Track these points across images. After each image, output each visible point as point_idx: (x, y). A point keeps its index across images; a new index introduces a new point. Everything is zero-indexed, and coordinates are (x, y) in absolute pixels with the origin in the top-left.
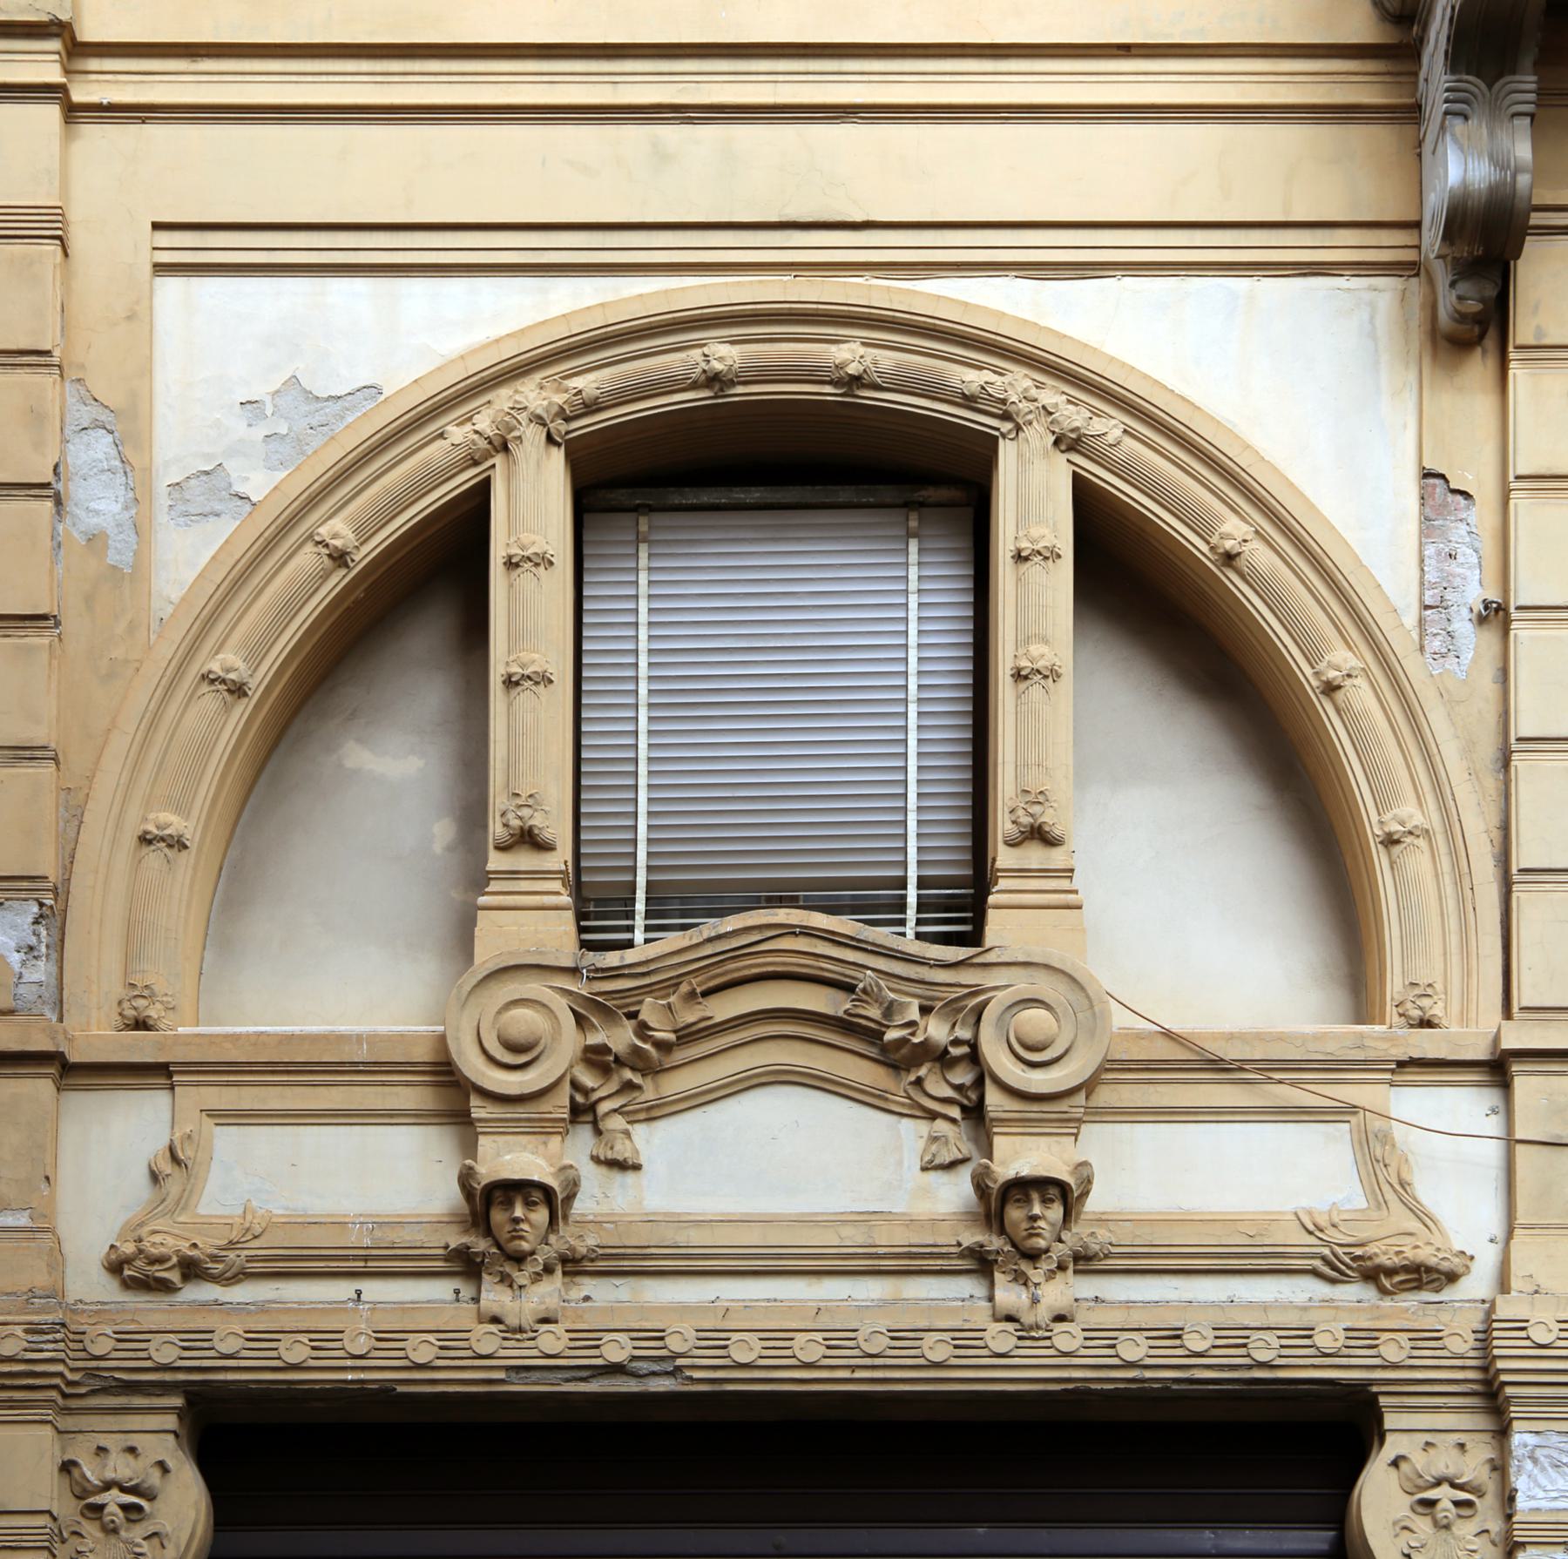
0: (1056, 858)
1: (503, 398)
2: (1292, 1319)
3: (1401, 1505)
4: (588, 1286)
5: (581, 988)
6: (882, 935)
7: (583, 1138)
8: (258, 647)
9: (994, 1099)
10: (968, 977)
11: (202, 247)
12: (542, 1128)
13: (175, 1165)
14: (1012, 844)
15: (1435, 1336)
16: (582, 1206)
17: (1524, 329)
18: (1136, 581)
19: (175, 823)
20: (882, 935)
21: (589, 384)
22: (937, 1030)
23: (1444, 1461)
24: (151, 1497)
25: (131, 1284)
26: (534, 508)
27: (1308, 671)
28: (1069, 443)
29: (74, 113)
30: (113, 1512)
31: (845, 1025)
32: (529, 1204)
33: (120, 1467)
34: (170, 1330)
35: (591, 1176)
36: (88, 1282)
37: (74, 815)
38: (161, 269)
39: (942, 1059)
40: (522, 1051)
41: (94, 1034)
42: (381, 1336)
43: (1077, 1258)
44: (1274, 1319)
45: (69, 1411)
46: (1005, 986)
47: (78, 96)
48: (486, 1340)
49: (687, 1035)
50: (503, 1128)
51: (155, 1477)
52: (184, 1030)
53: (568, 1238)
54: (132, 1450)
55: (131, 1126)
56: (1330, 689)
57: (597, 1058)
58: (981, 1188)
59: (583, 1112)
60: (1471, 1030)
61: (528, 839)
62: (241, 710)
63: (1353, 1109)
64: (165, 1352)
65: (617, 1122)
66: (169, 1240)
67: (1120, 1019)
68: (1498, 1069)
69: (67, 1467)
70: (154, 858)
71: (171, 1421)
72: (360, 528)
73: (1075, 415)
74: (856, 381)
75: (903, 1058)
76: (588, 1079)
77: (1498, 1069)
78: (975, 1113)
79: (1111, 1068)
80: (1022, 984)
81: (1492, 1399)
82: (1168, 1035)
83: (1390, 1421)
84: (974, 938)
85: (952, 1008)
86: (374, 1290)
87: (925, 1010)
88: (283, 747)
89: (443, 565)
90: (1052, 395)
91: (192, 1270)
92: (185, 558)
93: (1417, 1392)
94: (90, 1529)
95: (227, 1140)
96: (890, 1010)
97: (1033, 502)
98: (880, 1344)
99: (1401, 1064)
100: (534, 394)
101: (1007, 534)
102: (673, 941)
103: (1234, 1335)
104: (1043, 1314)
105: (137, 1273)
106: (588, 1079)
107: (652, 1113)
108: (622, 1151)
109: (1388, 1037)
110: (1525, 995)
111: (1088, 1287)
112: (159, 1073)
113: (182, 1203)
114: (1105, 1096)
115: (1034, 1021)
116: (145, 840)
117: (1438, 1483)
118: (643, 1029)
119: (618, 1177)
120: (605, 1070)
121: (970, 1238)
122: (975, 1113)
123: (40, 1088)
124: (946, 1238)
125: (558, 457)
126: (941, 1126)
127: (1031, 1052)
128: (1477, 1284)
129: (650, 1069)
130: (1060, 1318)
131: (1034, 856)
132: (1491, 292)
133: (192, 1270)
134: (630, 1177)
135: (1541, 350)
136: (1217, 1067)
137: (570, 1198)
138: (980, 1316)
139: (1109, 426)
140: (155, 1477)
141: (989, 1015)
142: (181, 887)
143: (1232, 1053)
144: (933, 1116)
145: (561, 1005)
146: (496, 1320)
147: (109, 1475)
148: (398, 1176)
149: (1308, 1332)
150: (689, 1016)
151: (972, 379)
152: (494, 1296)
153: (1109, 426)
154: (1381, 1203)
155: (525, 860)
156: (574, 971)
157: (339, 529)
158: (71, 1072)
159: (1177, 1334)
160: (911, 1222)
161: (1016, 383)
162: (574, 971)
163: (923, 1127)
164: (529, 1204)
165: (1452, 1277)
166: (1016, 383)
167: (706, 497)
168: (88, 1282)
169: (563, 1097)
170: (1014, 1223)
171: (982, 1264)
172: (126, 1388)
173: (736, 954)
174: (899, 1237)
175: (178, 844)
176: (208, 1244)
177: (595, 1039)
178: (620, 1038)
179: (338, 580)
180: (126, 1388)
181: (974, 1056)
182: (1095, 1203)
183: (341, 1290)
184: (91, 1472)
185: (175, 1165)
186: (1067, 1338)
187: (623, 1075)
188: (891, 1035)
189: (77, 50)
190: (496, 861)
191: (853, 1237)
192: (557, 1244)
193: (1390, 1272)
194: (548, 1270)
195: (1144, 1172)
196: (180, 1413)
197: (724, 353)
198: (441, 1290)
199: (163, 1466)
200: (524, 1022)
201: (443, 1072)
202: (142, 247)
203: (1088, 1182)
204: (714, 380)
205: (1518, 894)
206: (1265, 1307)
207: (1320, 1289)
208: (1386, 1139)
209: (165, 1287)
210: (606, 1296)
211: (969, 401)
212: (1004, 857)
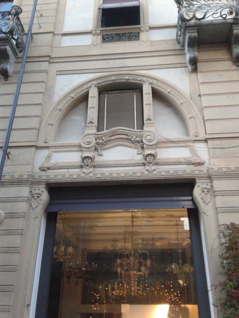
0: (152, 122)
1: (91, 83)
2: (183, 169)
3: (200, 192)
4: (96, 169)
5: (96, 136)
6: (134, 130)
7: (96, 153)
8: (64, 106)
9: (145, 146)
10: (141, 133)
11: (61, 73)
12: (91, 151)
13: (49, 157)
14: (146, 120)
15: (202, 171)
16: (95, 160)
17: (199, 70)
18: (157, 95)
19: (52, 123)
20: (134, 130)
21: (99, 81)
22: (138, 139)
23: (205, 186)
24: (41, 195)
25: (42, 170)
26: (94, 93)
27: (166, 92)
28: (150, 84)
29: (50, 63)
30: (36, 197)
31: (127, 139)
32: (89, 159)
33: (37, 191)
34: (44, 176)
35: (96, 156)
36: (37, 170)
37: (41, 123)
38: (57, 75)
39: (139, 142)
40: (89, 143)
41: (41, 144)
42: (70, 175)
43: (156, 163)
44: (181, 170)
45: (32, 185)
46: (145, 134)
47: (50, 61)
48: (83, 175)
49: (108, 141)
50: (86, 151)
51: (41, 193)
52: (50, 144)
53: (93, 163)
54: (39, 189)
55: (44, 153)
56: (169, 92)
57: (97, 144)
58: (144, 156)
59: (96, 149)
60: (202, 136)
61: (91, 122)
62: (61, 112)
63: (189, 146)
64: (44, 178)
65: (100, 151)
66: (47, 165)
67: (160, 137)
68: (206, 141)
69: (31, 192)
70: (50, 126)
71: (44, 186)
72: (75, 95)
73: (151, 81)
74: (128, 80)
75: (133, 142)
76: (97, 146)
77: (206, 141)
78: (143, 148)
79: (159, 143)
80: (148, 134)
81: (210, 178)
82: (166, 139)
83: (197, 181)
84: (143, 129)
85: (139, 137)
86: (70, 170)
87: (136, 137)
88: (67, 117)
89: (84, 98)
90: (148, 79)
91: (49, 168)
92: (56, 98)
93: (201, 177)
94: (33, 199)
95: (55, 154)
96: (132, 137)
97: (147, 90)
98: (132, 174)
99: (194, 141)
100: (94, 83)
101: (144, 92)
102: (108, 131)
103: (176, 172)
104: (152, 170)
105: (42, 169)
106: (97, 146)
107: (104, 149)
108: (100, 153)
109: (192, 137)
110: (208, 132)
111: (157, 167)
112: (48, 147)
113: (49, 161)
114: (159, 146)
115: (148, 137)
116: (49, 124)
117: (204, 189)
118: (103, 140)
119: (100, 156)
120: (99, 145)
121: (142, 162)
122: (143, 148)
123: (33, 149)
124: (140, 162)
125: (96, 88)
126: (139, 150)
127: (150, 141)
128: (207, 165)
129: (104, 145)
130: (154, 170)
131: (149, 122)
132: (195, 67)
133: (49, 168)
134: (101, 157)
135: (201, 72)
136: (172, 142)
137: (94, 159)
138: (144, 171)
139: (155, 82)
140: (41, 193)
141: (144, 137)
142: (52, 130)
143: (174, 140)
144: (138, 148)
145: (94, 138)
146: (84, 173)
147: (36, 192)
148: (74, 157)
149: (185, 171)
150: (108, 139)
151: (140, 79)
152: (147, 168)
153: (155, 82)
154: (193, 156)
155: (91, 125)
156: (95, 134)
157: (73, 95)
158: (37, 148)
159: (169, 172)
160: (135, 160)
161: (144, 79)
162: (95, 134)
163: (137, 150)
164: (89, 159)
165: (203, 164)
166: (144, 79)
167: (111, 92)
168: (37, 170)
169: (93, 149)
170: (150, 159)
171: (144, 165)
172: (39, 183)
173: (114, 132)
174: (134, 162)
175: (52, 125)
176: (51, 166)
177: (98, 141)
178: (101, 141)
179: (72, 100)
180: (39, 183)
181: (142, 142)
182: (158, 157)
183: (66, 170)
184: (34, 192)
185: (49, 157)
186: (155, 173)
187: (99, 147)
188: (132, 140)
189: (51, 58)
190: (88, 125)
191: (128, 162)
192: (155, 161)
193: (195, 164)
194: (91, 167)
195: (164, 154)
196: (46, 185)
197: (113, 78)
198: (142, 167)
199: (43, 192)
200: (88, 140)
201: (80, 146)
202: (55, 73)
203: (156, 154)
204: (113, 80)
205: (206, 123)
206: (179, 168)
207: (187, 166)
208: (194, 149)
209: (45, 170)
210: (98, 170)
211: (140, 81)
212: (145, 122)
